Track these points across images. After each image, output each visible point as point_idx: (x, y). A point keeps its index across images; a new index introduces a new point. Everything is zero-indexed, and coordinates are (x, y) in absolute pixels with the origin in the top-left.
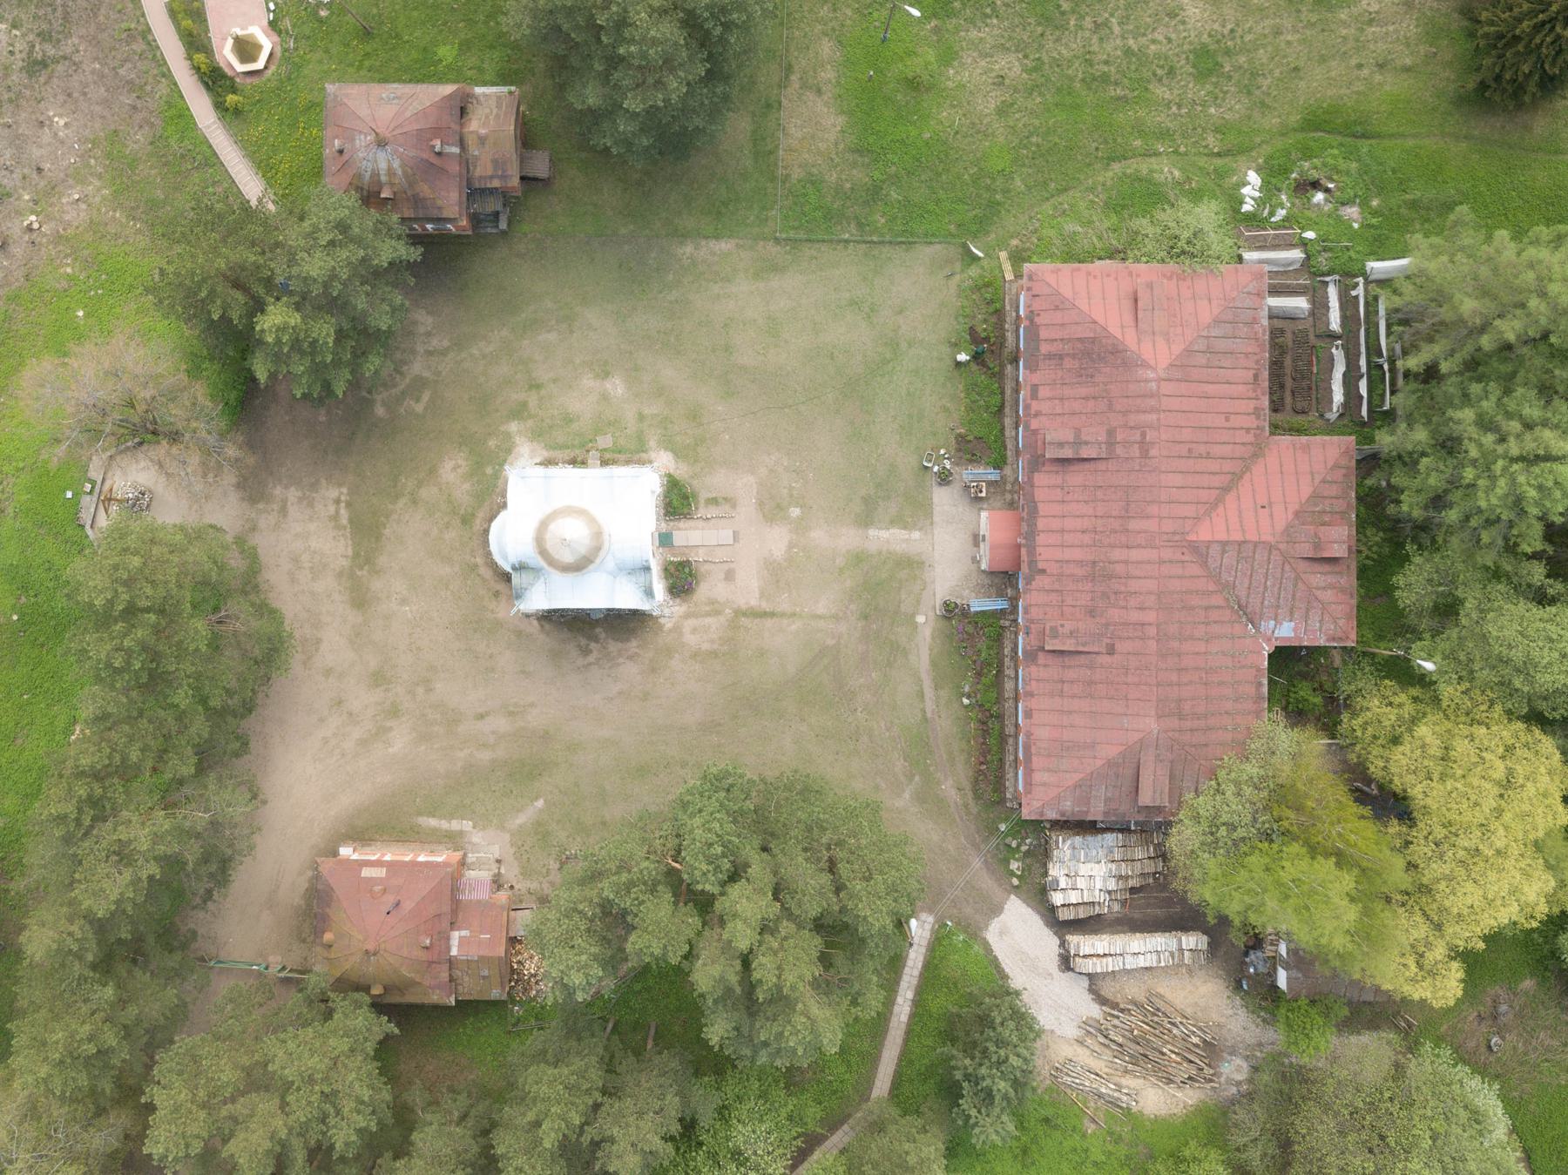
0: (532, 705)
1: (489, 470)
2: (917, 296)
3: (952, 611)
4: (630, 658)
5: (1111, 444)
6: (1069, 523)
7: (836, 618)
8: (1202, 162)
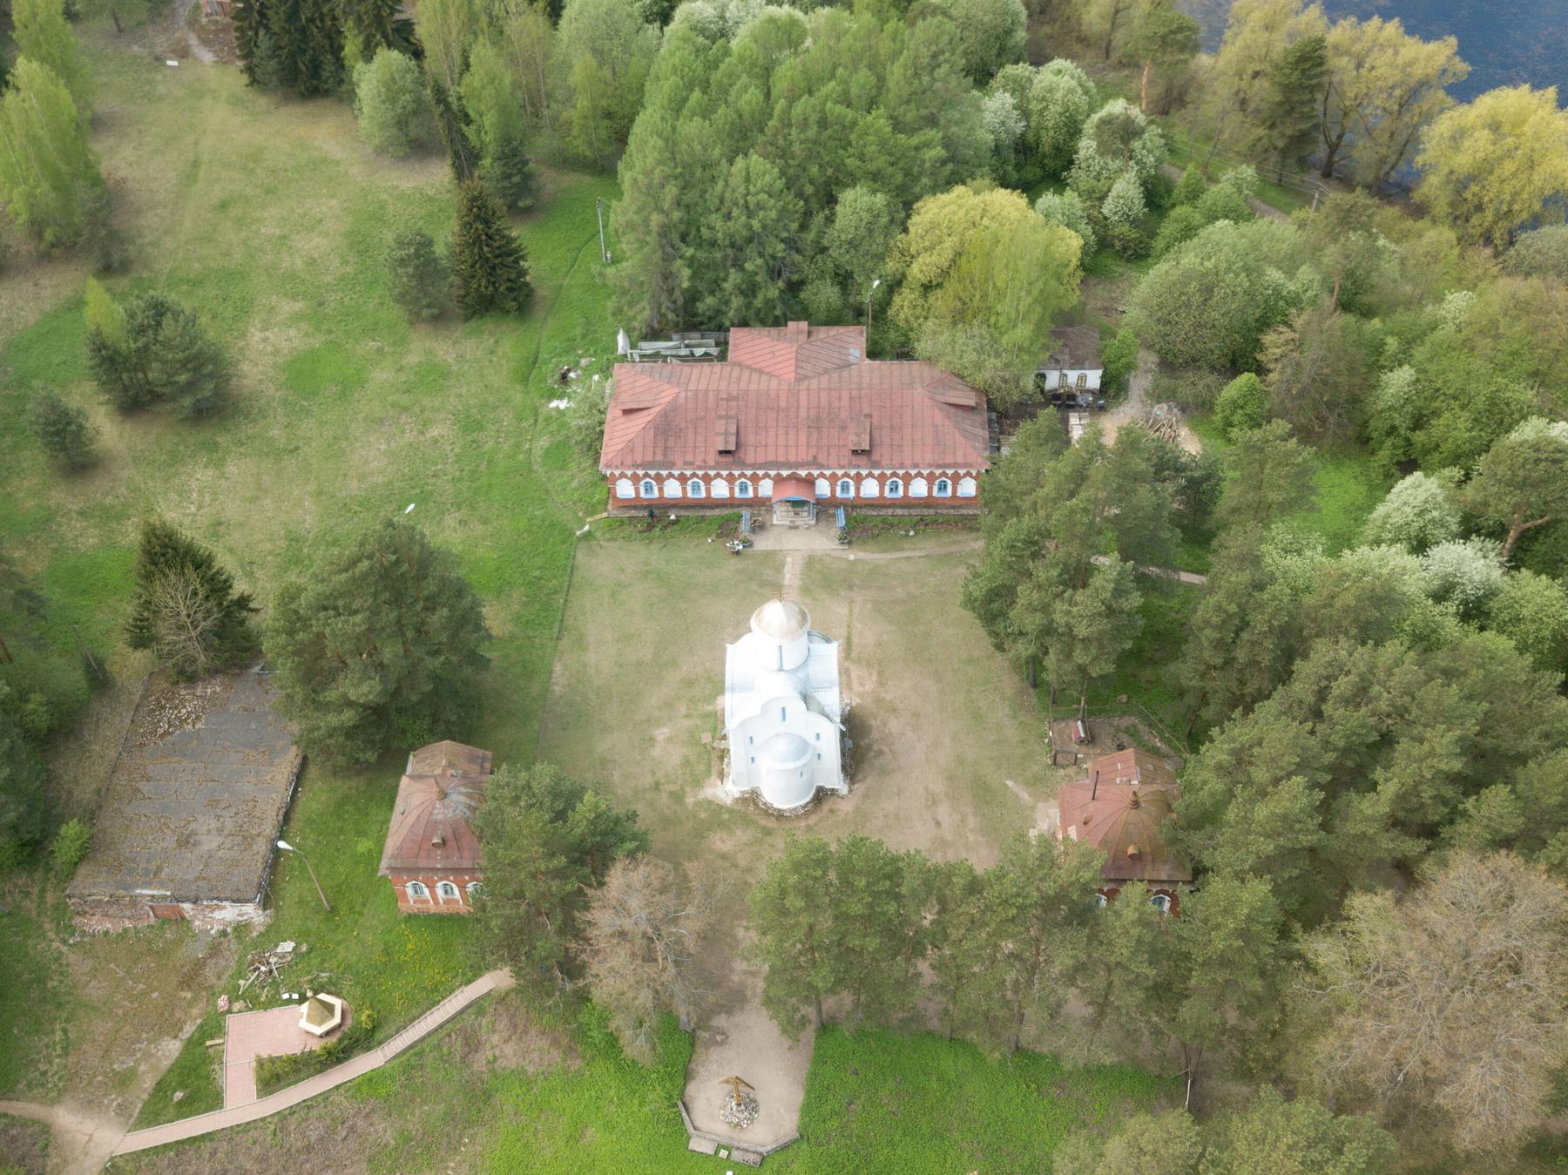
0: (926, 789)
1: (726, 816)
2: (613, 566)
3: (847, 538)
4: (885, 724)
5: (727, 417)
6: (782, 442)
7: (851, 602)
8: (539, 428)
